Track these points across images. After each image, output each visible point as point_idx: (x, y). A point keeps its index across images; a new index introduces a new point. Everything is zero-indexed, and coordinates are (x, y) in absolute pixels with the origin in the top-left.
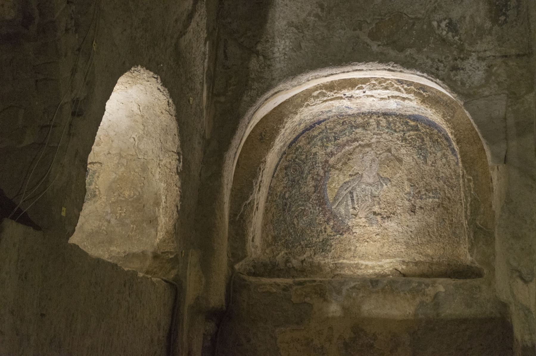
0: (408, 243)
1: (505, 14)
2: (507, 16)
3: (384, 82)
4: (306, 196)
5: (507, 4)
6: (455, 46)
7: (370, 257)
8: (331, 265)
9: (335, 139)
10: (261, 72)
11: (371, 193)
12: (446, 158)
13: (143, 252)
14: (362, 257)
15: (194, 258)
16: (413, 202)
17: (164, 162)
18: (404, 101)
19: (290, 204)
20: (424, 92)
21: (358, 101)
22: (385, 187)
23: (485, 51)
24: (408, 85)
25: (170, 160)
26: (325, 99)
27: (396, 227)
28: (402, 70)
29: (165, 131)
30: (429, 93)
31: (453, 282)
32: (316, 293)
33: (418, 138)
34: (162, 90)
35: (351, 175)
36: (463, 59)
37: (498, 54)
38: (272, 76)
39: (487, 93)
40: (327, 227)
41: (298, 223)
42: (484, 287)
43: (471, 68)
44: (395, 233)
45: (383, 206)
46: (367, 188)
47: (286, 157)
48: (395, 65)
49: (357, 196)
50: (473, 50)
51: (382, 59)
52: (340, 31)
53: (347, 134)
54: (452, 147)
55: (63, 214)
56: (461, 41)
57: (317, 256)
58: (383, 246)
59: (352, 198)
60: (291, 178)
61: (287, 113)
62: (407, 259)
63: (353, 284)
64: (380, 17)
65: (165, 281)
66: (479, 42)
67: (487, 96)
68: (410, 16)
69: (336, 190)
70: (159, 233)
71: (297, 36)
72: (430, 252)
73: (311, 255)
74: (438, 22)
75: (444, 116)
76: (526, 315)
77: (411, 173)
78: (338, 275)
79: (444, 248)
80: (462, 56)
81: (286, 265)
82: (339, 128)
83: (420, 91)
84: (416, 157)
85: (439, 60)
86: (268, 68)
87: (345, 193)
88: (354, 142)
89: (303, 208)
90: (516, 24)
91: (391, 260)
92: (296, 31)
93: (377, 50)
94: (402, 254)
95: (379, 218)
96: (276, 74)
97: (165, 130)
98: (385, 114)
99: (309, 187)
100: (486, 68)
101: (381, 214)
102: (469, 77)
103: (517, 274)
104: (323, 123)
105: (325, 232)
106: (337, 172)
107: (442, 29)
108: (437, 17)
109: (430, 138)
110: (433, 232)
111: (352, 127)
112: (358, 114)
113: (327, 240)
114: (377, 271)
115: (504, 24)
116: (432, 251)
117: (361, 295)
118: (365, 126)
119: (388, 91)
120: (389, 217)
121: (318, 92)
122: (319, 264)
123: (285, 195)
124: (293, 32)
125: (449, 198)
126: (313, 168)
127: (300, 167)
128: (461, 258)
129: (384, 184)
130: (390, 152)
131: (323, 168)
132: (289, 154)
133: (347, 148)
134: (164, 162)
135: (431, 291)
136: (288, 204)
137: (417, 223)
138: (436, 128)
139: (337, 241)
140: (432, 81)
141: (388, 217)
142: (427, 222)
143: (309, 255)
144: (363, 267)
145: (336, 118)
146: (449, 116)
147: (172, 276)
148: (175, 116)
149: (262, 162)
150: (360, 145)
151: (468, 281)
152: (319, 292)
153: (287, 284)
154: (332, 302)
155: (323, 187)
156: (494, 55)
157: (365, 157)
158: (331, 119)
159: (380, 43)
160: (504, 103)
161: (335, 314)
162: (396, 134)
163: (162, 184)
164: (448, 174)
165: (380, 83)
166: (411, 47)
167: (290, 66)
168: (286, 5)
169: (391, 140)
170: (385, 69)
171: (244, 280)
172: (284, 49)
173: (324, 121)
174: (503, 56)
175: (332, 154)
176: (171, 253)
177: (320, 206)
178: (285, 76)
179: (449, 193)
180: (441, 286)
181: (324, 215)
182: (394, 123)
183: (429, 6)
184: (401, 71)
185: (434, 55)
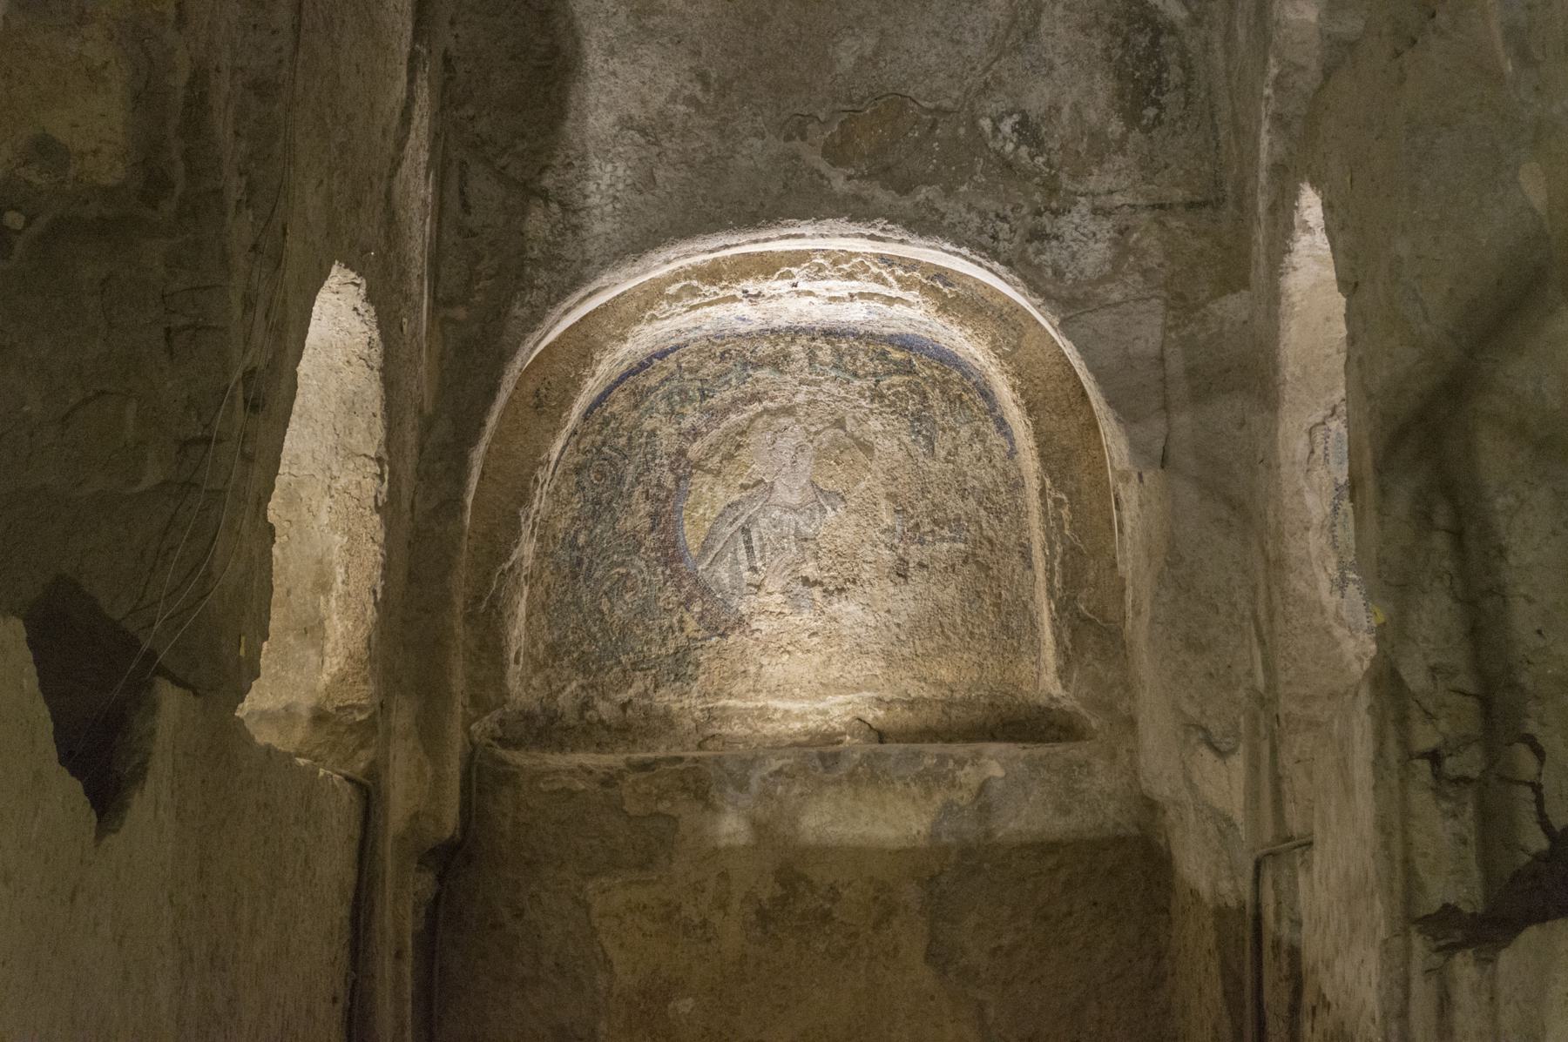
0: (890, 654)
1: (1155, 103)
2: (1161, 108)
5: (1159, 78)
6: (1037, 179)
8: (697, 714)
9: (704, 397)
10: (556, 244)
11: (797, 530)
12: (983, 441)
13: (286, 709)
15: (403, 716)
16: (900, 551)
17: (343, 481)
18: (890, 305)
19: (591, 562)
20: (946, 285)
21: (774, 304)
22: (831, 514)
23: (1111, 192)
24: (906, 269)
25: (360, 478)
26: (697, 301)
27: (861, 613)
28: (906, 237)
29: (351, 407)
31: (1024, 753)
32: (685, 789)
33: (912, 391)
34: (362, 311)
35: (744, 487)
36: (1056, 213)
37: (1141, 201)
38: (583, 253)
39: (1116, 296)
40: (687, 617)
41: (611, 610)
42: (1099, 764)
43: (1075, 234)
44: (858, 630)
45: (825, 562)
46: (786, 517)
47: (578, 443)
48: (890, 226)
49: (761, 539)
50: (1082, 189)
51: (857, 211)
52: (752, 140)
53: (734, 382)
54: (998, 412)
55: (242, 652)
56: (1051, 167)
57: (662, 691)
58: (828, 662)
59: (748, 542)
60: (590, 495)
61: (601, 338)
62: (888, 695)
63: (775, 765)
64: (849, 107)
65: (348, 779)
66: (1096, 171)
67: (1117, 304)
68: (925, 104)
69: (707, 525)
70: (327, 660)
71: (644, 153)
72: (945, 674)
75: (994, 345)
77: (895, 479)
79: (980, 665)
80: (1054, 205)
81: (582, 717)
82: (712, 367)
83: (936, 284)
84: (906, 440)
85: (997, 215)
86: (575, 234)
87: (730, 530)
88: (750, 402)
89: (623, 570)
90: (1184, 128)
91: (850, 697)
92: (642, 141)
93: (846, 188)
95: (817, 592)
96: (593, 249)
97: (349, 404)
98: (830, 334)
99: (637, 517)
101: (821, 584)
102: (1073, 256)
103: (1201, 735)
104: (672, 356)
105: (682, 630)
106: (709, 478)
107: (1005, 139)
108: (992, 107)
109: (943, 392)
111: (745, 364)
112: (762, 334)
114: (811, 725)
115: (1154, 126)
116: (954, 674)
117: (796, 790)
118: (778, 363)
119: (854, 283)
120: (843, 590)
121: (678, 286)
122: (667, 710)
123: (575, 538)
124: (634, 143)
125: (990, 541)
126: (648, 470)
127: (613, 465)
128: (1025, 688)
130: (843, 428)
131: (672, 470)
132: (584, 435)
133: (733, 417)
134: (343, 481)
135: (969, 776)
136: (586, 561)
138: (958, 367)
139: (712, 653)
140: (980, 265)
141: (841, 590)
142: (936, 601)
144: (778, 715)
145: (704, 342)
147: (362, 765)
148: (381, 370)
149: (541, 464)
150: (766, 410)
151: (1059, 748)
152: (693, 787)
153: (610, 768)
154: (725, 812)
155: (674, 517)
156: (1131, 202)
158: (693, 346)
159: (851, 171)
160: (1160, 321)
161: (732, 841)
162: (857, 383)
163: (337, 538)
165: (835, 263)
167: (628, 228)
168: (614, 74)
169: (844, 399)
170: (862, 236)
171: (504, 763)
173: (673, 350)
175: (695, 434)
176: (361, 709)
177: (666, 564)
178: (616, 254)
179: (992, 527)
180: (996, 762)
181: (679, 587)
182: (852, 356)
183: (970, 80)
184: (902, 241)
185: (984, 203)
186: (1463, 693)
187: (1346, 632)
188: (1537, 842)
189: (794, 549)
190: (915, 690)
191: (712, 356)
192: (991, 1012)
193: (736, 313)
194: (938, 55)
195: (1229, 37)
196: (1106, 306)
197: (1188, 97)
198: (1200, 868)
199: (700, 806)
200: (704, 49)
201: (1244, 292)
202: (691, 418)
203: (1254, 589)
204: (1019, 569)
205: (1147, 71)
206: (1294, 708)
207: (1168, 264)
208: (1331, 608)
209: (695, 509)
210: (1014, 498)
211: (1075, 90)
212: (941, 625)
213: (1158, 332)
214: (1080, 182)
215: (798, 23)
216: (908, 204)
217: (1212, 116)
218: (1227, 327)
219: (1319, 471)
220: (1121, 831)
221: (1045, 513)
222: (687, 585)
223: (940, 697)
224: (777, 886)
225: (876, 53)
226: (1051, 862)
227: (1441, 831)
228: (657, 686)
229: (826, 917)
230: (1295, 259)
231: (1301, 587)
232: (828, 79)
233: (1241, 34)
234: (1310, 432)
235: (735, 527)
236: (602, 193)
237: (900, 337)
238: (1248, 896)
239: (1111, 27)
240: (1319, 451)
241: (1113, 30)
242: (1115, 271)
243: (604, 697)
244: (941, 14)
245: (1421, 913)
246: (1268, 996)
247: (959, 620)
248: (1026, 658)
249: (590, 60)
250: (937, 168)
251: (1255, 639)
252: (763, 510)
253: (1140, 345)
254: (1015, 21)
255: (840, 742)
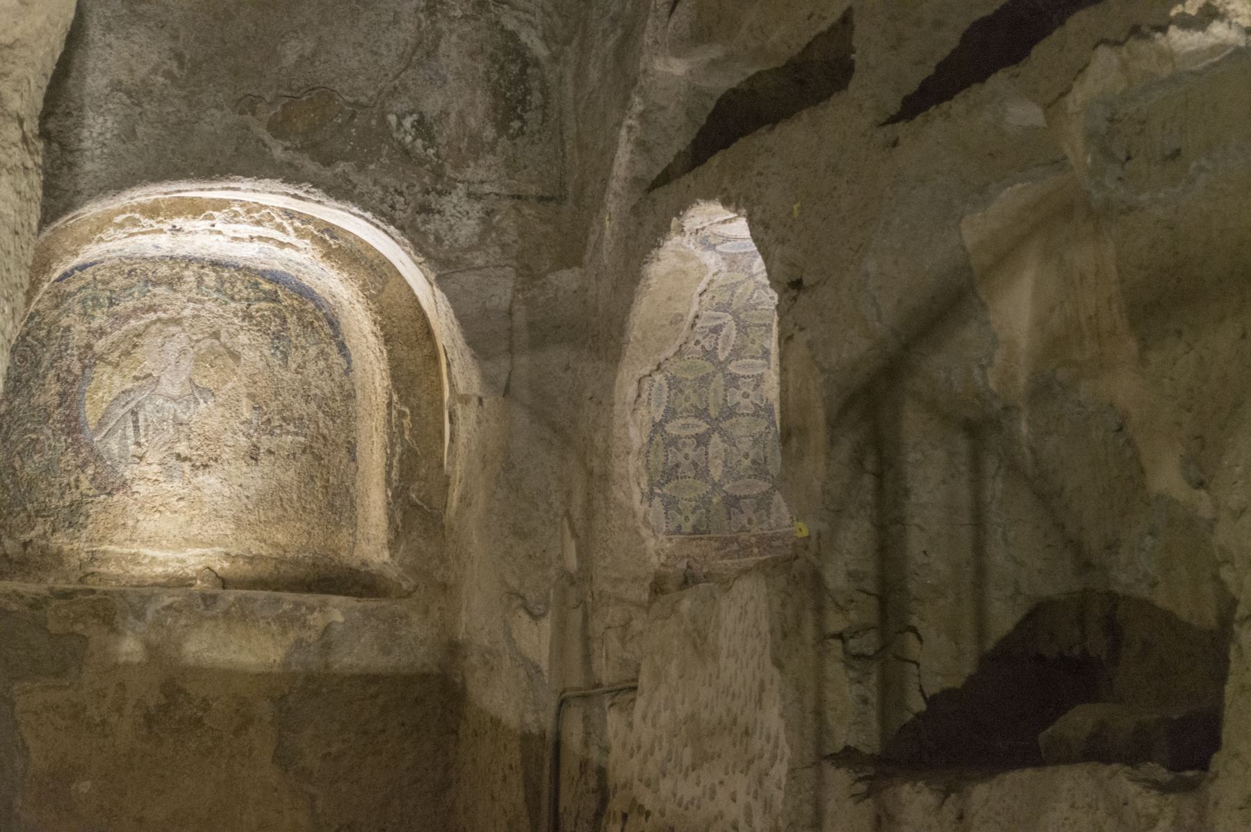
0: (239, 519)
1: (520, 118)
2: (524, 122)
3: (258, 212)
4: (42, 413)
5: (524, 99)
6: (428, 166)
7: (164, 542)
8: (83, 555)
9: (111, 304)
10: (56, 175)
11: (175, 416)
12: (326, 360)
14: (146, 542)
19: (9, 427)
20: (332, 237)
22: (203, 405)
23: (482, 182)
24: (303, 222)
27: (219, 485)
30: (341, 242)
32: (96, 616)
33: (275, 316)
35: (136, 378)
36: (440, 194)
37: (504, 191)
38: (75, 185)
39: (479, 262)
40: (82, 477)
41: (22, 467)
42: (415, 617)
43: (453, 211)
44: (216, 499)
45: (195, 443)
46: (167, 405)
49: (146, 420)
51: (290, 175)
52: (213, 111)
53: (136, 295)
54: (340, 338)
57: (58, 535)
58: (190, 522)
59: (136, 422)
61: (59, 252)
62: (234, 551)
63: (167, 601)
64: (288, 94)
66: (472, 164)
67: (479, 268)
68: (348, 98)
69: (104, 406)
72: (280, 538)
73: (45, 533)
74: (398, 117)
76: (529, 677)
77: (255, 383)
78: (93, 573)
79: (309, 533)
80: (439, 187)
82: (120, 281)
84: (267, 352)
85: (396, 190)
87: (121, 412)
88: (148, 311)
92: (128, 102)
94: (226, 540)
96: (82, 183)
98: (215, 264)
100: (481, 214)
101: (190, 460)
102: (451, 228)
103: (520, 601)
104: (90, 270)
105: (77, 487)
106: (109, 369)
107: (406, 132)
108: (398, 107)
109: (299, 319)
110: (291, 500)
112: (163, 259)
113: (80, 504)
114: (170, 570)
116: (287, 539)
117: (182, 622)
118: (173, 283)
121: (124, 216)
122: (60, 551)
125: (324, 437)
126: (61, 358)
127: (34, 352)
128: (342, 554)
129: (201, 401)
130: (218, 338)
131: (80, 360)
133: (133, 322)
135: (316, 620)
137: (260, 481)
138: (313, 300)
139: (100, 508)
140: (378, 227)
141: (206, 466)
143: (41, 532)
144: (146, 561)
146: (375, 288)
150: (159, 319)
154: (125, 635)
155: (78, 397)
156: (497, 191)
157: (168, 345)
158: (108, 263)
159: (288, 144)
160: (511, 284)
161: (130, 659)
162: (233, 305)
164: (327, 390)
165: (248, 212)
166: (347, 160)
167: (112, 169)
168: (109, 45)
169: (221, 316)
170: (287, 194)
172: (101, 134)
174: (513, 197)
175: (102, 333)
177: (68, 434)
178: (101, 189)
179: (327, 426)
180: (337, 610)
181: (77, 453)
182: (231, 283)
184: (319, 202)
185: (387, 180)
186: (869, 594)
187: (650, 532)
188: (918, 705)
189: (172, 431)
190: (256, 549)
191: (121, 273)
192: (319, 803)
193: (155, 241)
194: (360, 61)
195: (580, 75)
196: (471, 268)
197: (545, 115)
198: (502, 700)
199: (106, 629)
200: (182, 34)
201: (576, 269)
202: (100, 319)
203: (569, 494)
204: (345, 461)
205: (515, 91)
206: (607, 587)
207: (520, 241)
208: (640, 514)
209: (96, 392)
210: (346, 405)
211: (461, 101)
212: (281, 500)
213: (509, 291)
214: (460, 173)
215: (257, 25)
216: (329, 174)
217: (561, 133)
218: (561, 294)
219: (643, 411)
220: (426, 670)
221: (389, 421)
222: (84, 453)
223: (275, 555)
224: (162, 696)
225: (314, 54)
226: (373, 689)
227: (847, 693)
228: (54, 531)
229: (199, 722)
230: (662, 252)
231: (620, 496)
232: (276, 70)
233: (594, 74)
234: (639, 381)
235: (126, 409)
236: (93, 139)
237: (272, 273)
238: (549, 726)
239: (492, 55)
240: (644, 396)
241: (493, 59)
242: (481, 242)
243: (10, 536)
244: (365, 30)
245: (828, 751)
246: (566, 800)
247: (295, 497)
248: (344, 530)
249: (91, 32)
250: (353, 148)
251: (568, 533)
252: (150, 398)
253: (496, 300)
254: (420, 43)
255: (191, 585)
